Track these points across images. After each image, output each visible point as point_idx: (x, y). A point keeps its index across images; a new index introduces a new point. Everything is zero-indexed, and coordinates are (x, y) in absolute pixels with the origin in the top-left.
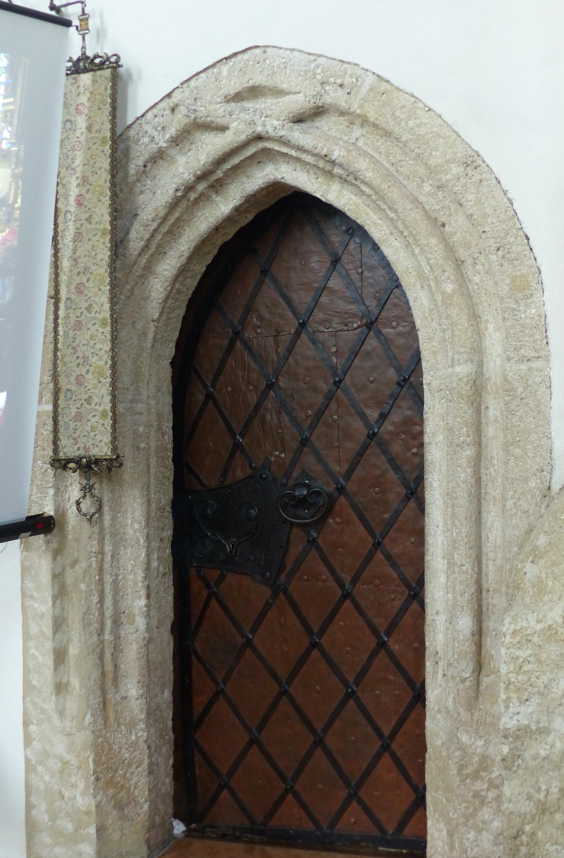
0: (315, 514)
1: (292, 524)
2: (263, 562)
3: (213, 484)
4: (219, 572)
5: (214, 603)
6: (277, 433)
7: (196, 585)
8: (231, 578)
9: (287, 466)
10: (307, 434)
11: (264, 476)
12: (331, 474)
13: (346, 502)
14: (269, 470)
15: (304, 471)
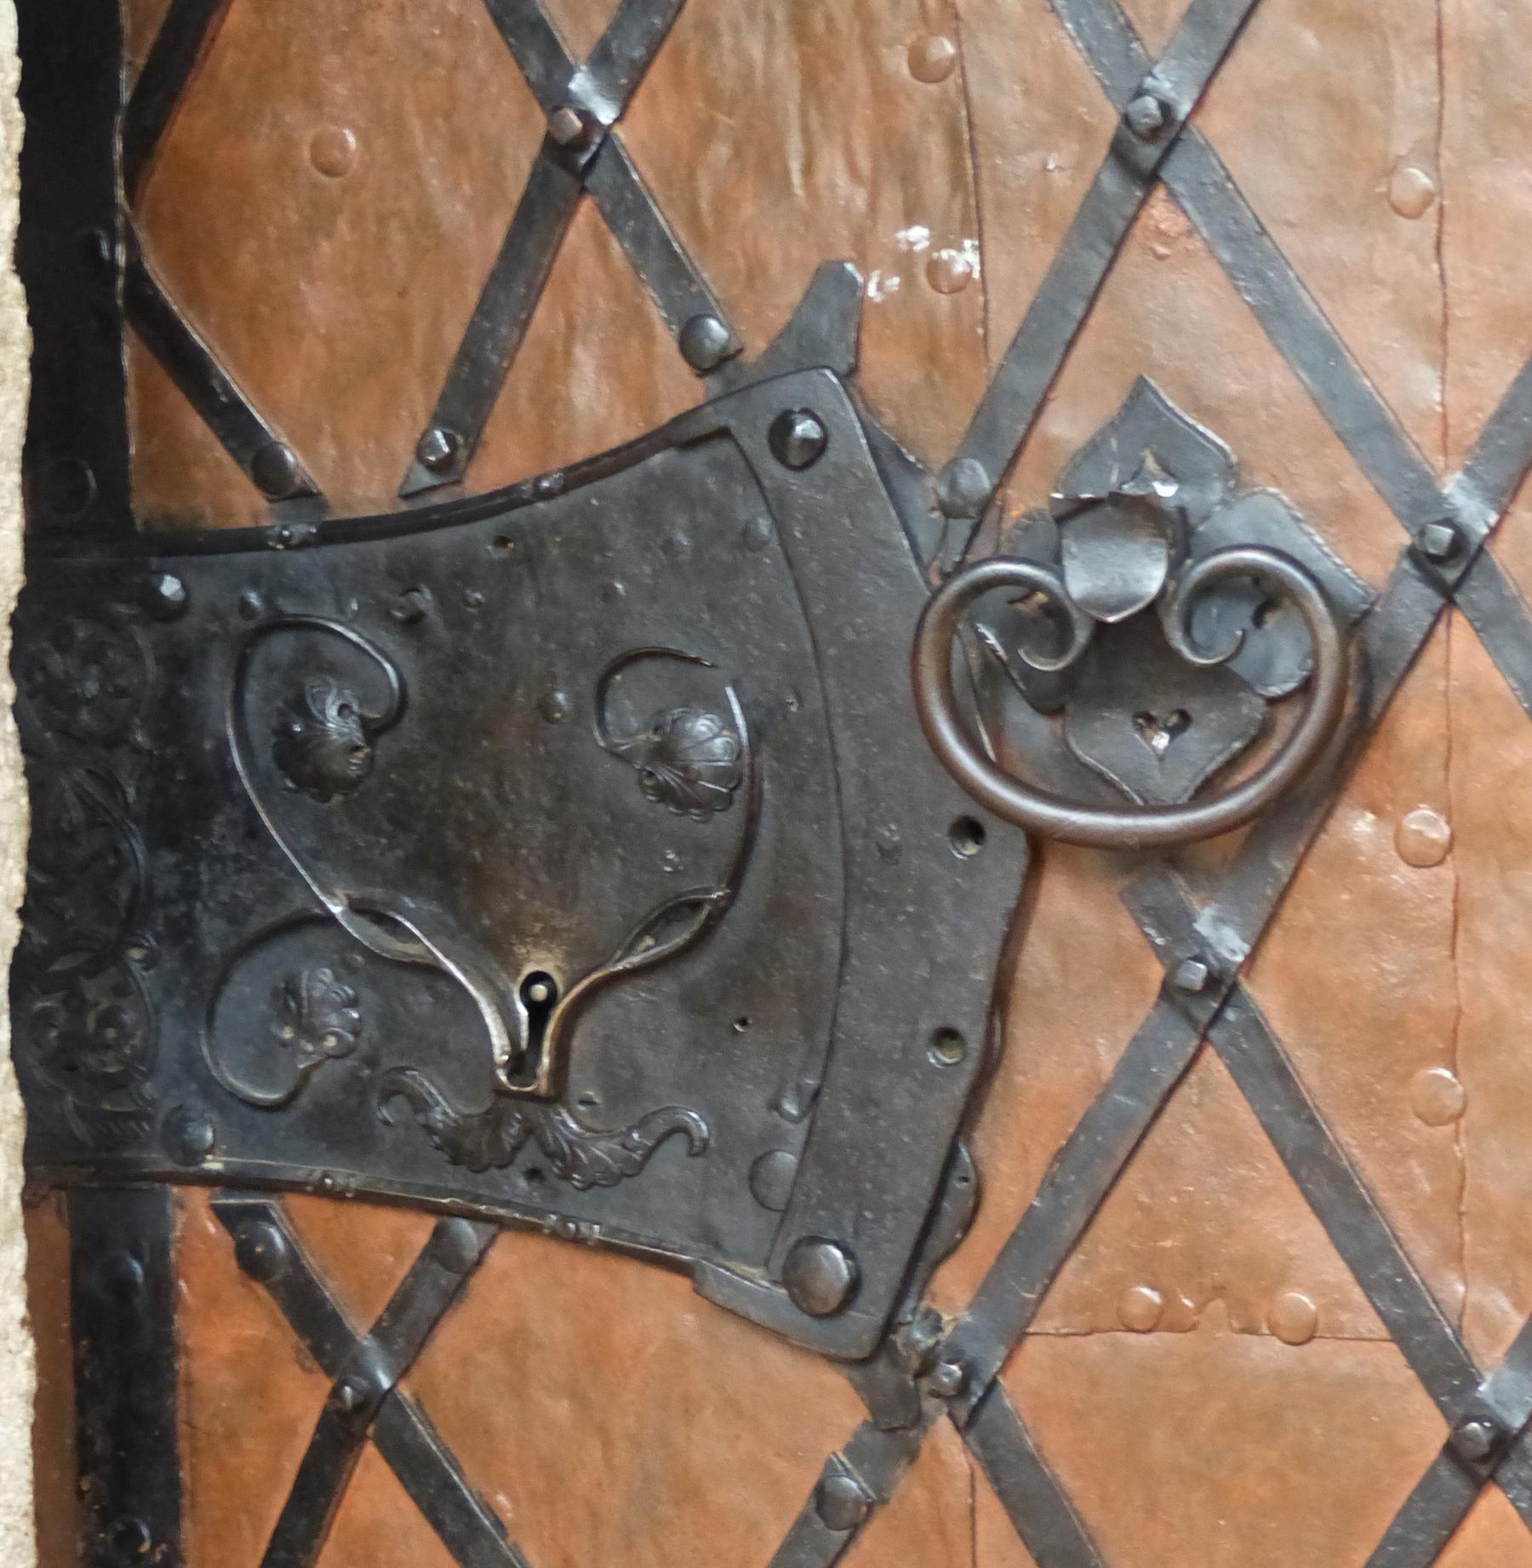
0: (1233, 764)
1: (1040, 845)
2: (787, 1159)
3: (365, 471)
4: (420, 1231)
5: (373, 1490)
6: (919, 65)
7: (224, 1337)
8: (519, 1280)
9: (996, 357)
10: (1170, 84)
11: (805, 428)
12: (1368, 430)
13: (1501, 684)
14: (849, 376)
15: (1139, 395)
